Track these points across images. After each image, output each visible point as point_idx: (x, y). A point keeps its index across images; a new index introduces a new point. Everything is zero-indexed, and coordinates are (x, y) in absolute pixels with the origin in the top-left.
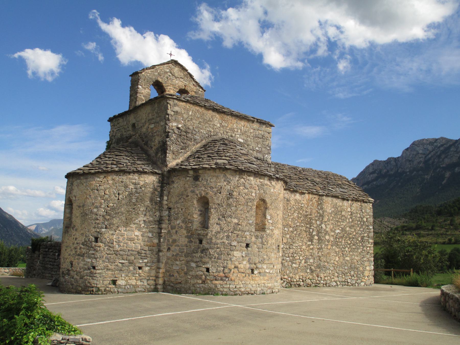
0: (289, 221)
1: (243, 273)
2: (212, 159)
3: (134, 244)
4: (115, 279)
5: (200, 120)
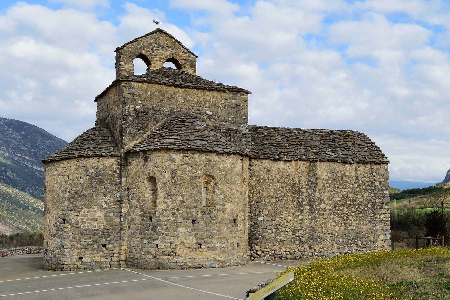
0: (271, 192)
1: (190, 248)
3: (97, 224)
4: (82, 257)
5: (161, 98)
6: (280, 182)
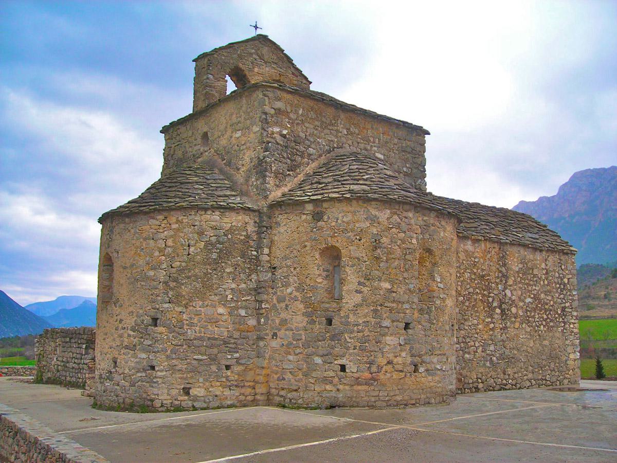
2: (342, 184)
3: (216, 329)
4: (188, 386)
6: (468, 271)
